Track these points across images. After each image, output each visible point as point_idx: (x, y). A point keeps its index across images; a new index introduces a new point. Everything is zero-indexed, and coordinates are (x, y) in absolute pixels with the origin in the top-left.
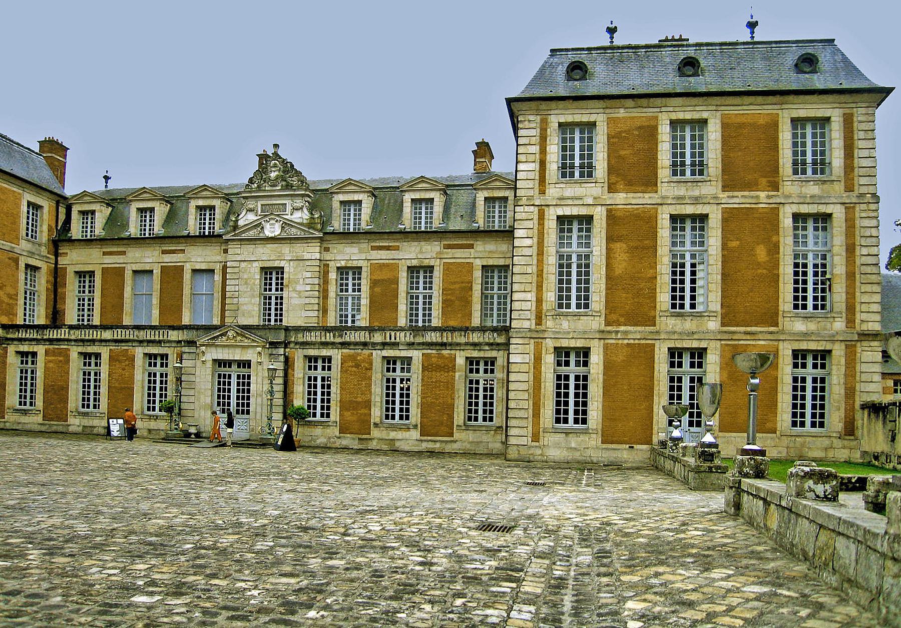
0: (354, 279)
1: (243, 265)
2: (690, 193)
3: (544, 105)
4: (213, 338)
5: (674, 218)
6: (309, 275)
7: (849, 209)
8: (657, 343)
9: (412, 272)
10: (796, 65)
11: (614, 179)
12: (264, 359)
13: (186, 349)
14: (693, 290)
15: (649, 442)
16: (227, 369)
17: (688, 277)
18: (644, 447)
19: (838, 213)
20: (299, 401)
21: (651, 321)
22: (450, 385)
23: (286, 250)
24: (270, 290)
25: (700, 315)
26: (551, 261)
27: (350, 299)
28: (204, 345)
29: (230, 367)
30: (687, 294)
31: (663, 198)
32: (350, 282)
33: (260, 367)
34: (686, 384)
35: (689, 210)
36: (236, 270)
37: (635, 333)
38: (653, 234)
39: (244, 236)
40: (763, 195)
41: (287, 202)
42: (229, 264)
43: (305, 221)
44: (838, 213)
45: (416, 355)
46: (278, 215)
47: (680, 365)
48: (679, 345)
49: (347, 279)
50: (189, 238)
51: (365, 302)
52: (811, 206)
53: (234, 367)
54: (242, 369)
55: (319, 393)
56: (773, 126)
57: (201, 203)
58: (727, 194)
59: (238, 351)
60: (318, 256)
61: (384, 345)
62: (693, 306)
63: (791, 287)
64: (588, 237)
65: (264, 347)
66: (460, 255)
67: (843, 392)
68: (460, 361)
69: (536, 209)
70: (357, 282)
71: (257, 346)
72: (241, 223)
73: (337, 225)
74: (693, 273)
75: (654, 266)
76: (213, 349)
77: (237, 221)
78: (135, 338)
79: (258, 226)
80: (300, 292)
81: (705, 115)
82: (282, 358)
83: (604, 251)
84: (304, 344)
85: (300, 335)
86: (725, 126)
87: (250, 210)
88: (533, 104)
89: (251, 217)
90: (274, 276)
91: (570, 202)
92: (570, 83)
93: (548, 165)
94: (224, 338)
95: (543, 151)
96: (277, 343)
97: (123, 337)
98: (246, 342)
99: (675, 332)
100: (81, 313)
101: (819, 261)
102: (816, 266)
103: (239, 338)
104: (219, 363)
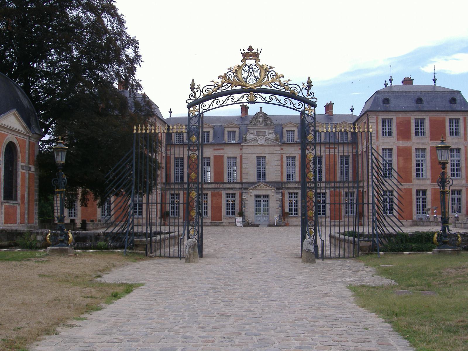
0: (292, 160)
1: (249, 155)
2: (421, 142)
3: (377, 113)
4: (255, 187)
5: (416, 149)
6: (276, 159)
8: (413, 188)
9: (229, 132)
10: (450, 101)
11: (399, 137)
12: (274, 194)
13: (244, 191)
14: (422, 171)
15: (411, 219)
16: (259, 198)
17: (421, 167)
18: (411, 220)
20: (287, 210)
21: (411, 181)
23: (267, 149)
24: (260, 165)
25: (425, 179)
27: (291, 168)
28: (251, 190)
29: (260, 197)
30: (421, 170)
31: (413, 143)
33: (273, 197)
34: (421, 201)
35: (421, 147)
36: (247, 157)
38: (410, 154)
39: (249, 144)
41: (267, 130)
42: (243, 155)
43: (274, 138)
45: (328, 191)
46: (263, 136)
47: (419, 195)
48: (419, 189)
49: (289, 161)
50: (225, 144)
52: (456, 146)
53: (262, 197)
54: (265, 198)
55: (231, 209)
56: (444, 121)
57: (230, 129)
58: (431, 142)
59: (264, 191)
60: (279, 152)
62: (422, 176)
63: (450, 170)
64: (391, 155)
65: (274, 190)
67: (465, 202)
69: (376, 146)
70: (289, 162)
71: (272, 190)
72: (247, 138)
73: (285, 140)
74: (422, 166)
75: (411, 164)
76: (254, 191)
77: (246, 137)
78: (222, 187)
79: (255, 140)
80: (273, 166)
81: (425, 117)
82: (281, 194)
83: (397, 160)
84: (288, 188)
85: (286, 185)
86: (431, 121)
87: (252, 133)
88: (374, 112)
89: (252, 136)
90: (261, 160)
91: (386, 144)
92: (385, 105)
93: (379, 132)
94: (259, 187)
95: (377, 127)
96: (279, 188)
97: (217, 187)
98: (268, 188)
99: (418, 185)
100: (177, 175)
101: (458, 162)
102: (457, 164)
103: (265, 187)
104: (257, 196)
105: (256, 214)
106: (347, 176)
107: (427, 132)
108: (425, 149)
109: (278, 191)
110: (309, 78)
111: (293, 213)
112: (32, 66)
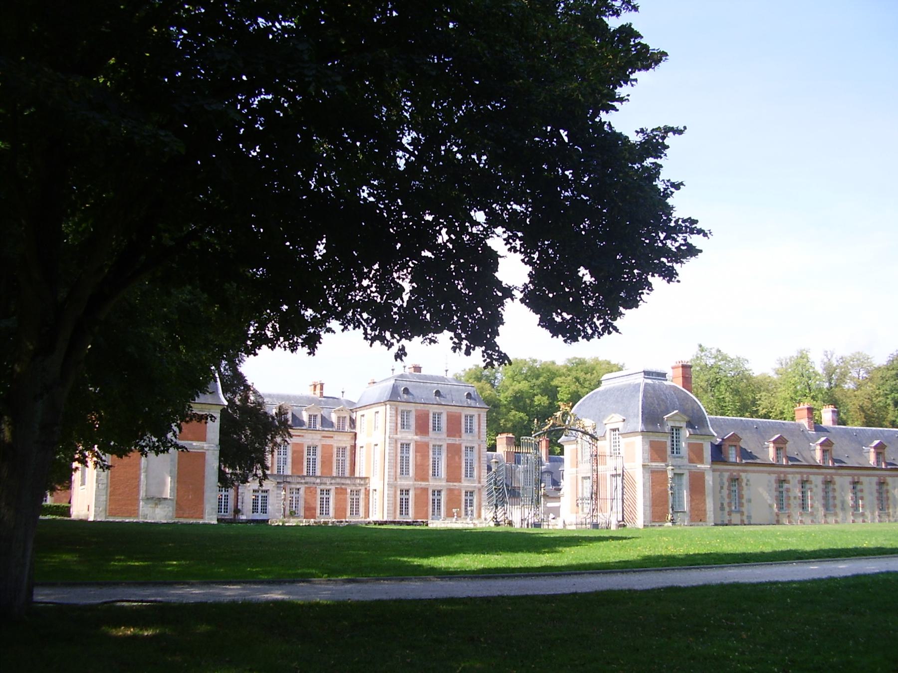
7: (479, 445)
12: (275, 489)
19: (476, 446)
22: (345, 500)
26: (399, 458)
32: (282, 450)
35: (438, 443)
37: (424, 484)
40: (457, 439)
44: (476, 446)
51: (289, 460)
61: (321, 484)
66: (328, 442)
68: (349, 491)
75: (429, 461)
105: (253, 512)
106: (343, 471)
107: (444, 428)
108: (441, 446)
109: (279, 485)
110: (624, 364)
111: (223, 511)
112: (460, 323)
